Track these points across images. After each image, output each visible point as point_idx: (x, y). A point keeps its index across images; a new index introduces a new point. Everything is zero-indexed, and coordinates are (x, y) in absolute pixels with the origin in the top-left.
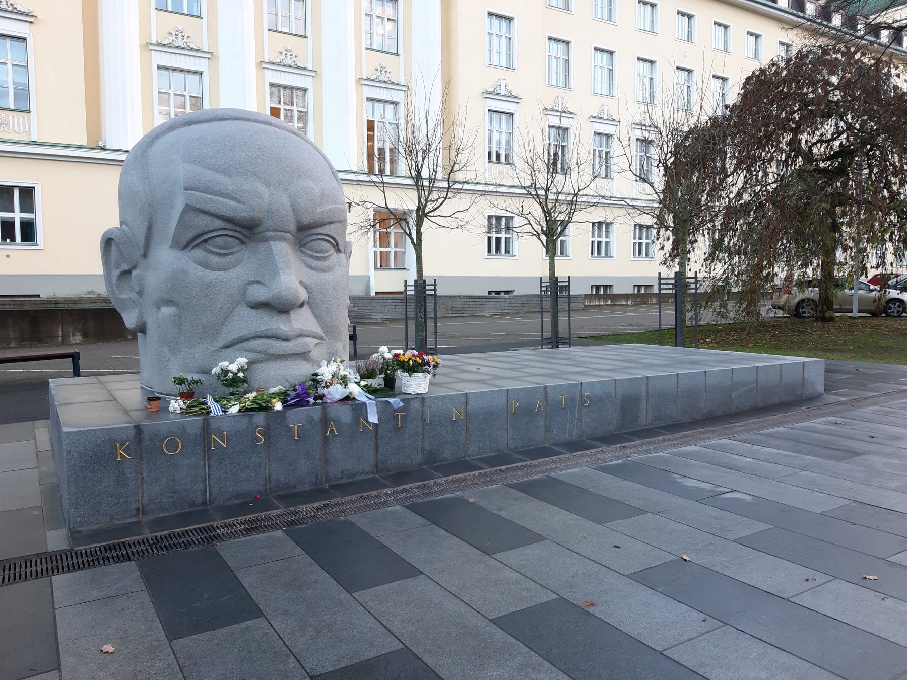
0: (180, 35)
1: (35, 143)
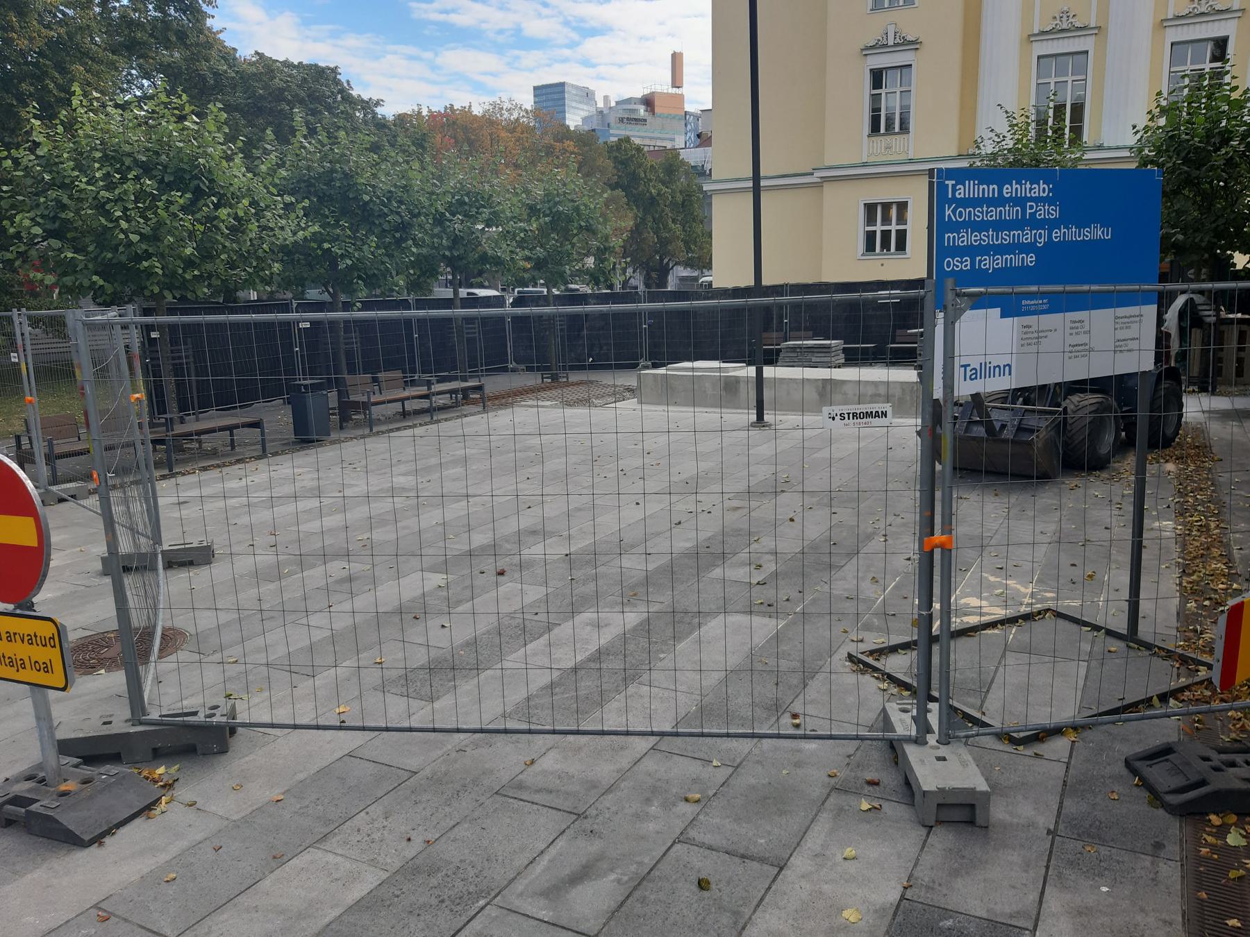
0: (1065, 16)
1: (911, 161)
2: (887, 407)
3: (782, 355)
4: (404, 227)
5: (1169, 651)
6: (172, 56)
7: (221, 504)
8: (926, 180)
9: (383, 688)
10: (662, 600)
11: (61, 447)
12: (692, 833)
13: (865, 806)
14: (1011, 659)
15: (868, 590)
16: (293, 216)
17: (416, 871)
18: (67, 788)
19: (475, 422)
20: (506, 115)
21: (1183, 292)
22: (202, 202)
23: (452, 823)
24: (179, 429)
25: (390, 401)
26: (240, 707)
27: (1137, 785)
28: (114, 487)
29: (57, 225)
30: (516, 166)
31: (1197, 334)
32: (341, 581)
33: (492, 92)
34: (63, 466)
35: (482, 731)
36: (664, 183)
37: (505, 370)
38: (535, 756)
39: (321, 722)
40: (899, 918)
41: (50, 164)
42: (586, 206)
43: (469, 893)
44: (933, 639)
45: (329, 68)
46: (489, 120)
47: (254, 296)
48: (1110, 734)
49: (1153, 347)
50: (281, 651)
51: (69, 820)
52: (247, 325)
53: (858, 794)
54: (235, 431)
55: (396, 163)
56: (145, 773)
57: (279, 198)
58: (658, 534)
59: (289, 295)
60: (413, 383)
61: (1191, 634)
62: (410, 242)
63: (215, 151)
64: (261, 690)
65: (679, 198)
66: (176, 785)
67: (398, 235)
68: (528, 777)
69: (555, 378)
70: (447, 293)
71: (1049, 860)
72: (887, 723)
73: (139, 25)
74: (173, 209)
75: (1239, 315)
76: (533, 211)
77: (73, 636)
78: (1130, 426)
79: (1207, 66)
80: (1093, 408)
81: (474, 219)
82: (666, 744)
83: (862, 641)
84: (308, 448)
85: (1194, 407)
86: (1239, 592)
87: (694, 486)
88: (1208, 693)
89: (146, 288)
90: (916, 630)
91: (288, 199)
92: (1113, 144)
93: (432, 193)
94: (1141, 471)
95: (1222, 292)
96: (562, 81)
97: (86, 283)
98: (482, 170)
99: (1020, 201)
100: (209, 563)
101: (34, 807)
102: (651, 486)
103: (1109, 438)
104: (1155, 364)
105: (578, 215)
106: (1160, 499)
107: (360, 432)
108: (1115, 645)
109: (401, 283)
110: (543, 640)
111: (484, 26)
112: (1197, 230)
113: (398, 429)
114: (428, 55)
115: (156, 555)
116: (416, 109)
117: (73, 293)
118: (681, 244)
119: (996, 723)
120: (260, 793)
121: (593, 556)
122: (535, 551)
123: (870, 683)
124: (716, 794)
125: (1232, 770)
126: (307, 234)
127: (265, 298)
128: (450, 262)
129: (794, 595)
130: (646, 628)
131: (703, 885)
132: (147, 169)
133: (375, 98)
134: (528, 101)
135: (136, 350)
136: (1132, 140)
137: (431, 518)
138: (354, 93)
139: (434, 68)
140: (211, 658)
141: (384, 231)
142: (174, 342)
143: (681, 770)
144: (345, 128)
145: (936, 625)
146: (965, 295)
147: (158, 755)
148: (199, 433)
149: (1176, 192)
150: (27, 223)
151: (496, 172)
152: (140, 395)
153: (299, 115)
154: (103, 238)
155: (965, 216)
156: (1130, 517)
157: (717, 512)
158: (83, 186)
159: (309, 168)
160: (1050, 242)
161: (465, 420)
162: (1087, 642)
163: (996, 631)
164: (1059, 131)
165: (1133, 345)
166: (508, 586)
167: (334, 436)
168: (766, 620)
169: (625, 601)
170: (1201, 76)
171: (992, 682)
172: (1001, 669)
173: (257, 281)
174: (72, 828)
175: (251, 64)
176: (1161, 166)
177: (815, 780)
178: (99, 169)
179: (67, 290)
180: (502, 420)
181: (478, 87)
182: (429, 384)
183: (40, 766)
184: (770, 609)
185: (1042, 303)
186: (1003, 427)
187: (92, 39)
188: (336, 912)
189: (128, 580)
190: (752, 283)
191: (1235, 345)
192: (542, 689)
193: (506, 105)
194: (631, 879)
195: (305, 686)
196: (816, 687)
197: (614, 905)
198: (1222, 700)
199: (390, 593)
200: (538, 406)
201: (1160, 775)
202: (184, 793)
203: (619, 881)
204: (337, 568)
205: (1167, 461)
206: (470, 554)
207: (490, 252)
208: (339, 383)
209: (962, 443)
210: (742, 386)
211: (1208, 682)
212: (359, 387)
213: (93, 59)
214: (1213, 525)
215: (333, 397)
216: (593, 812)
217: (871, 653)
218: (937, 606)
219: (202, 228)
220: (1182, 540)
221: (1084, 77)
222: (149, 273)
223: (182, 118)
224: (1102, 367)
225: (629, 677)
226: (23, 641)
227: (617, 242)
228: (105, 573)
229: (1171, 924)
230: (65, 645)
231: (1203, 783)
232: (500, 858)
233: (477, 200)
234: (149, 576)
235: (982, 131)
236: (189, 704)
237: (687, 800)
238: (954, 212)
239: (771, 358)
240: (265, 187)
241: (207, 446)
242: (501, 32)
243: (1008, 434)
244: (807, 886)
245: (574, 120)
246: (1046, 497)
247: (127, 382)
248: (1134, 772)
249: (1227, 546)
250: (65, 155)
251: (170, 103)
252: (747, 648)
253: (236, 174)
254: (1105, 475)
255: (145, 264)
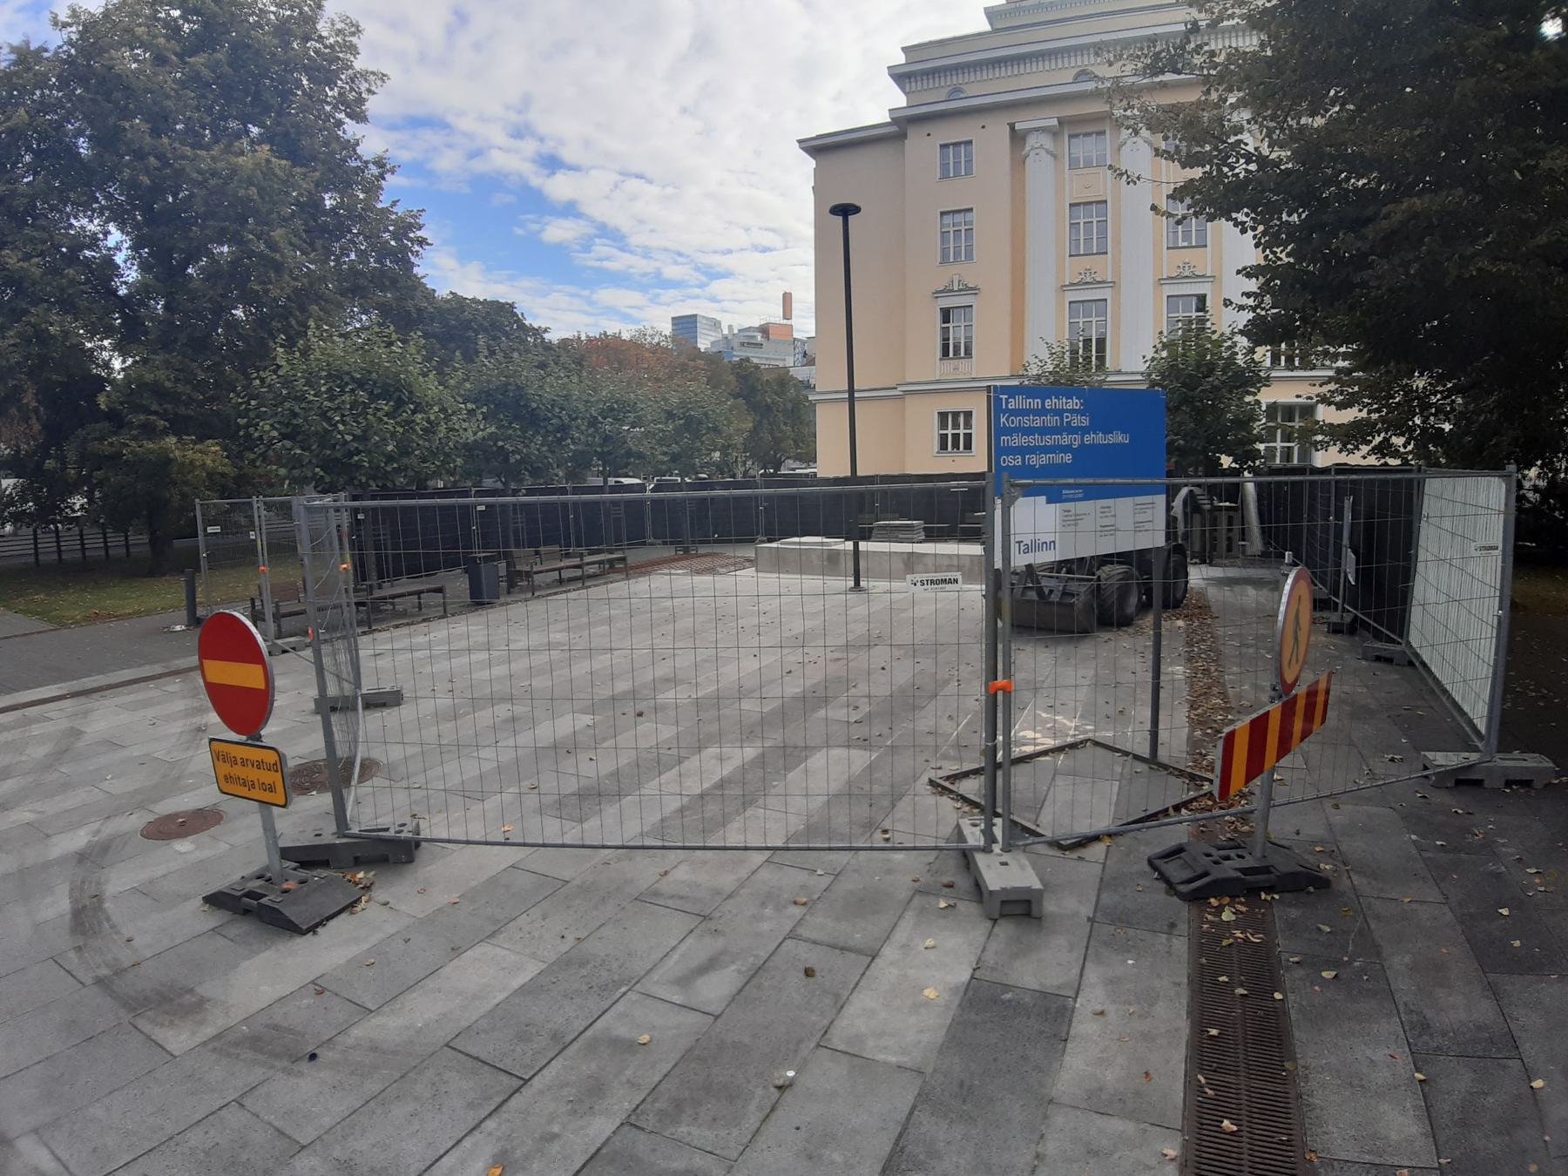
1: (974, 380)
2: (958, 576)
3: (875, 532)
4: (564, 429)
5: (1181, 771)
6: (385, 296)
7: (409, 656)
8: (985, 394)
9: (541, 811)
10: (775, 738)
11: (286, 607)
12: (800, 931)
13: (943, 904)
14: (1060, 781)
15: (946, 726)
16: (474, 419)
17: (569, 963)
18: (289, 887)
19: (619, 588)
20: (649, 339)
21: (1186, 485)
22: (402, 409)
23: (599, 924)
24: (377, 593)
25: (547, 571)
26: (422, 826)
27: (1156, 879)
28: (326, 641)
29: (289, 430)
30: (658, 380)
31: (1197, 517)
32: (506, 721)
33: (636, 321)
34: (287, 623)
35: (623, 847)
36: (776, 394)
37: (644, 544)
38: (667, 869)
39: (490, 839)
40: (970, 993)
41: (287, 382)
42: (713, 411)
43: (614, 981)
44: (997, 766)
45: (507, 304)
46: (634, 344)
47: (441, 484)
48: (1136, 838)
49: (1164, 527)
50: (457, 780)
51: (290, 912)
52: (432, 508)
53: (938, 895)
54: (422, 595)
55: (559, 378)
56: (349, 877)
57: (463, 406)
58: (772, 681)
59: (469, 484)
60: (568, 555)
61: (1198, 757)
62: (569, 441)
63: (414, 369)
64: (440, 812)
65: (789, 406)
66: (373, 887)
67: (559, 435)
68: (665, 886)
69: (686, 550)
70: (599, 482)
71: (1088, 942)
72: (960, 836)
73: (361, 273)
74: (379, 414)
75: (1227, 504)
76: (670, 415)
77: (292, 764)
78: (1149, 592)
79: (1194, 315)
80: (1121, 576)
81: (621, 422)
82: (779, 857)
83: (940, 768)
84: (480, 612)
85: (1197, 576)
86: (1232, 722)
87: (802, 641)
88: (1210, 803)
89: (356, 478)
90: (983, 758)
91: (470, 406)
92: (1129, 371)
93: (587, 402)
94: (1157, 626)
95: (1214, 485)
96: (694, 313)
97: (310, 474)
98: (629, 383)
99: (1059, 413)
100: (399, 704)
101: (264, 901)
102: (765, 641)
103: (1133, 601)
104: (1167, 541)
105: (707, 418)
106: (1174, 646)
107: (523, 596)
108: (1141, 767)
109: (561, 474)
110: (675, 771)
111: (631, 270)
112: (1194, 438)
113: (556, 594)
114: (586, 293)
115: (357, 698)
116: (576, 334)
117: (299, 483)
118: (792, 442)
119: (1048, 834)
120: (440, 897)
121: (718, 700)
122: (667, 697)
123: (947, 803)
124: (819, 898)
125: (1227, 862)
126: (485, 433)
127: (449, 486)
128: (601, 456)
129: (886, 731)
130: (761, 761)
131: (809, 973)
132: (361, 384)
133: (543, 326)
134: (667, 329)
135: (345, 528)
136: (1143, 368)
137: (581, 668)
138: (527, 323)
139: (591, 303)
140: (399, 785)
141: (547, 431)
142: (375, 522)
143: (791, 879)
144: (518, 350)
145: (1000, 755)
146: (1018, 485)
147: (358, 863)
148: (394, 597)
149: (1177, 408)
150: (267, 428)
151: (640, 385)
152: (347, 566)
153: (482, 341)
154: (324, 438)
155: (1016, 423)
156: (1150, 663)
157: (821, 662)
158: (312, 398)
159: (488, 382)
160: (1082, 445)
161: (610, 586)
162: (1118, 765)
163: (1047, 758)
164: (1088, 359)
165: (1148, 526)
166: (645, 726)
167: (502, 599)
168: (862, 752)
169: (744, 737)
170: (1190, 322)
171: (1044, 801)
172: (1052, 789)
173: (443, 472)
174: (293, 919)
175: (447, 301)
176: (1164, 387)
177: (902, 885)
178: (324, 384)
179: (294, 481)
180: (641, 586)
181: (626, 318)
182: (581, 556)
183: (267, 868)
184: (865, 743)
185: (1079, 493)
186: (1051, 592)
187: (327, 285)
188: (505, 994)
189: (334, 718)
190: (849, 474)
191: (1225, 527)
192: (675, 812)
193: (650, 332)
194: (749, 970)
195: (476, 808)
196: (904, 805)
197: (734, 990)
198: (1221, 808)
199: (545, 732)
200: (670, 574)
201: (1175, 871)
202: (379, 894)
203: (739, 971)
204: (503, 710)
205: (1178, 619)
206: (613, 698)
207: (634, 448)
208: (507, 556)
209: (1017, 605)
210: (842, 557)
211: (1210, 795)
212: (524, 559)
213: (326, 301)
214: (1213, 669)
215: (502, 565)
216: (717, 914)
217: (948, 778)
218: (1000, 738)
219: (401, 430)
220: (1191, 681)
221: (1104, 318)
222: (358, 466)
223: (390, 344)
224: (1126, 544)
225: (747, 802)
226: (253, 765)
227: (738, 440)
228: (317, 712)
229: (1179, 985)
230: (285, 770)
231: (1206, 874)
232: (639, 953)
233: (624, 407)
234: (350, 714)
235: (1028, 357)
236: (383, 821)
237: (795, 903)
238: (1007, 420)
239: (867, 535)
240: (453, 397)
241: (399, 608)
242: (645, 275)
243: (1055, 598)
244: (895, 971)
245: (703, 344)
246: (1086, 648)
247: (337, 552)
248: (1154, 868)
249: (1224, 685)
250: (299, 374)
251: (381, 332)
252: (846, 776)
253: (430, 387)
254: (1131, 630)
255: (356, 458)
